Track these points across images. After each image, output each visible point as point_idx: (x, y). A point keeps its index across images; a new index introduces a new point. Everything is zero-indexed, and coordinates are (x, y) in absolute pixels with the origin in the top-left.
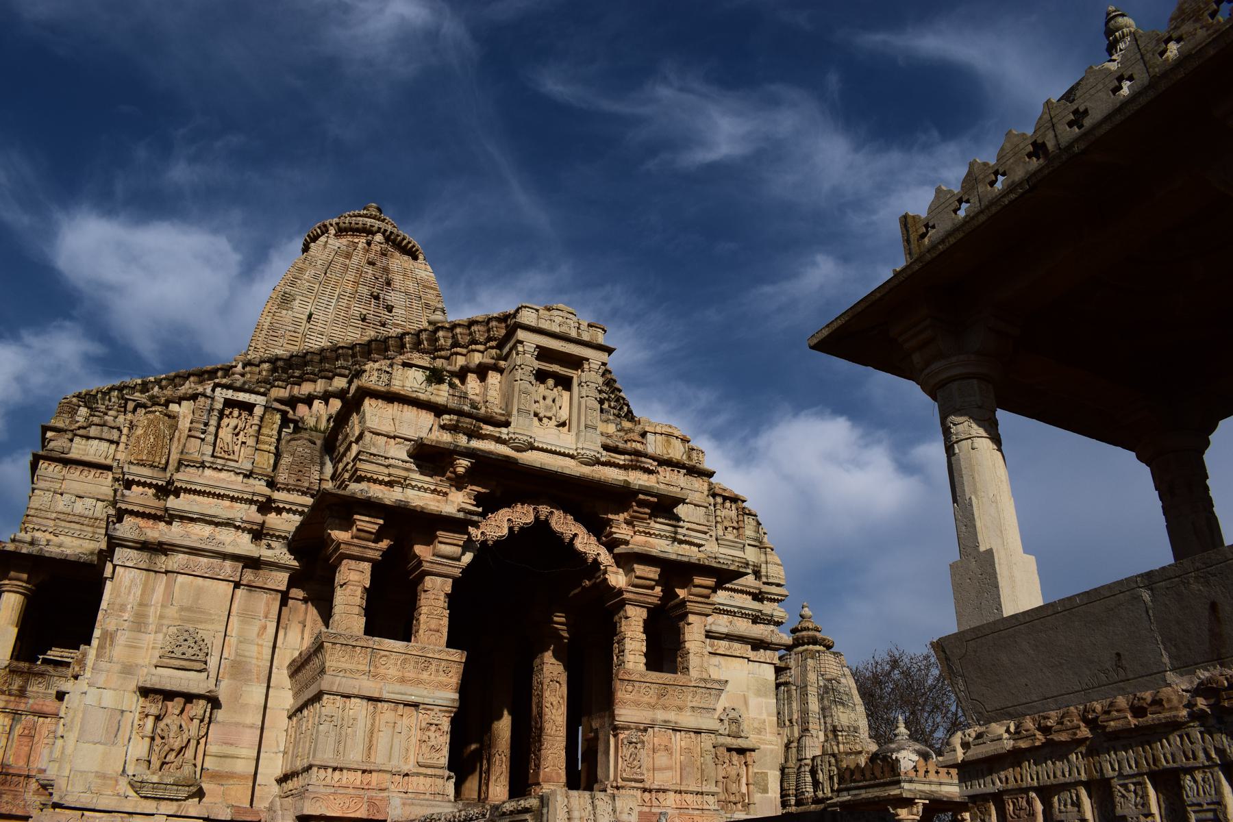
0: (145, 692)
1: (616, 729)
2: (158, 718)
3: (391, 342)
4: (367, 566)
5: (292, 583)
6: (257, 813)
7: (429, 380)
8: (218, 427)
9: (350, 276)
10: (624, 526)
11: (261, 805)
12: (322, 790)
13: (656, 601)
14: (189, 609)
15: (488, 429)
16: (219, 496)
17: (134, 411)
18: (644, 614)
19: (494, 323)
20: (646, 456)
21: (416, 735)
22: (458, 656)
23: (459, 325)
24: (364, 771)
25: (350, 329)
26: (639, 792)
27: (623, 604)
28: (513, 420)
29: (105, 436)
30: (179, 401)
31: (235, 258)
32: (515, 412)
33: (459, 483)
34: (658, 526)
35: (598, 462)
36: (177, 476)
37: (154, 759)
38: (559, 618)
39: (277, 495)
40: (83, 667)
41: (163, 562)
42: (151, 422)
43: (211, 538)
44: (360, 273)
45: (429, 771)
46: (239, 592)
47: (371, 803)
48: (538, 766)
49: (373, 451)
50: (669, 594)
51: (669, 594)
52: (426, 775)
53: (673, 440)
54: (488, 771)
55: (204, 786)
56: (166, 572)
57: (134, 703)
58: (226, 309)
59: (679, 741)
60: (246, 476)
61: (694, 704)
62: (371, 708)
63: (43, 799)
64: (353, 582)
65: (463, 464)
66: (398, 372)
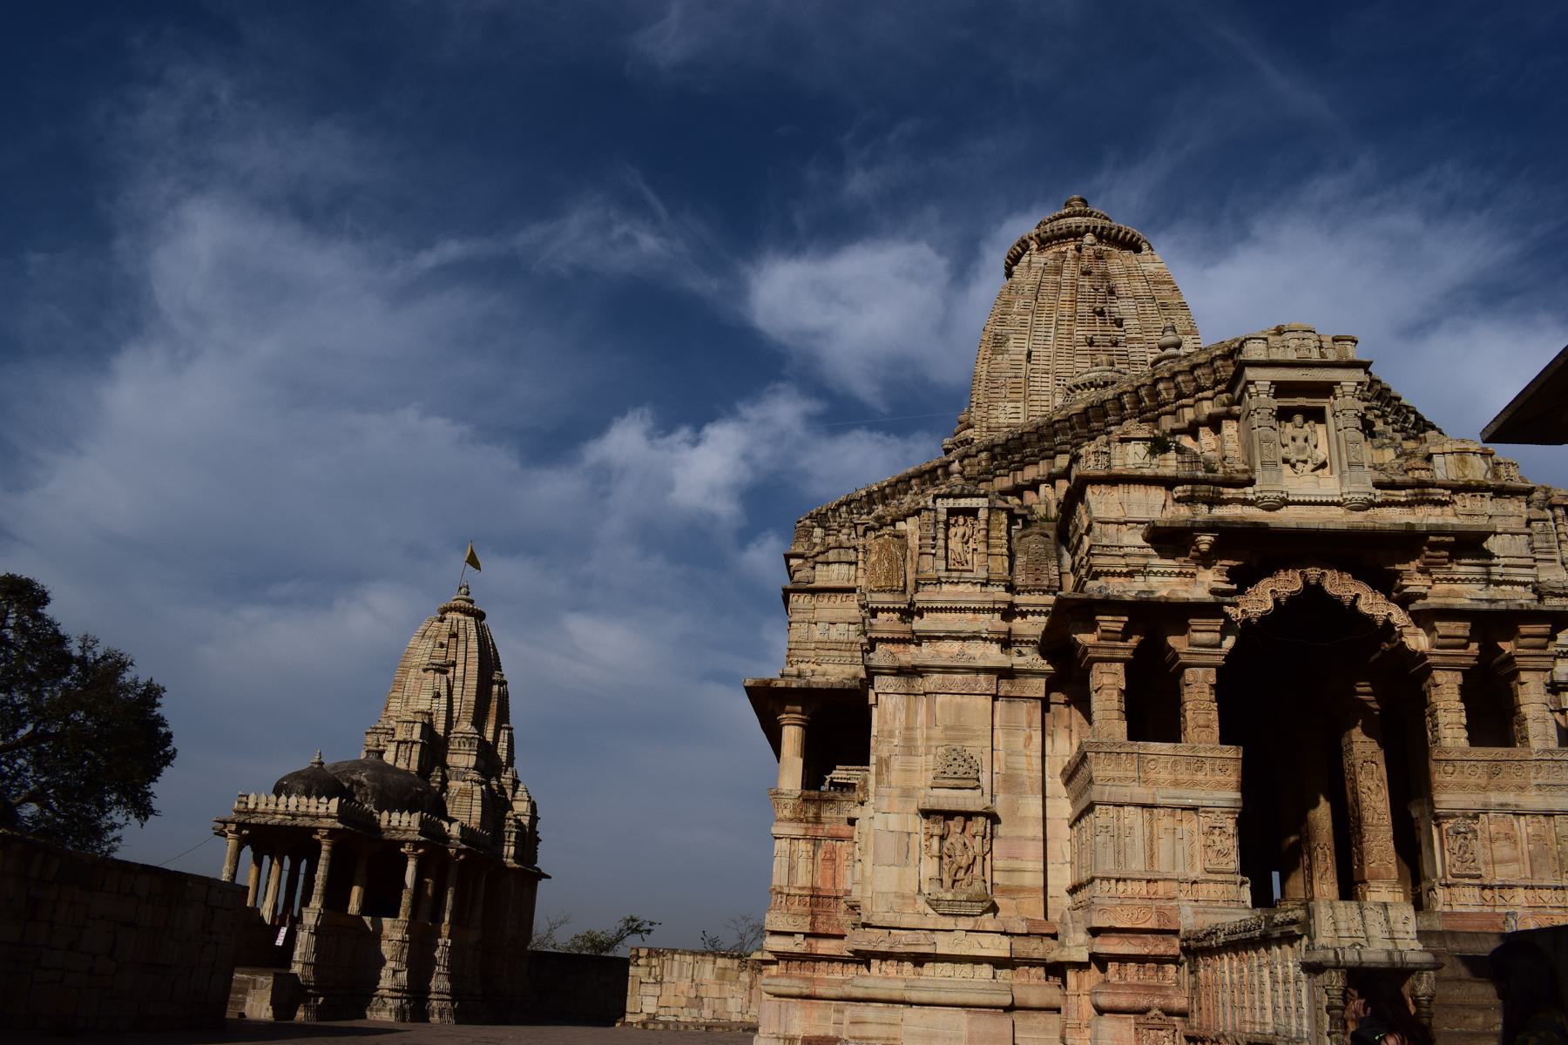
0: (926, 814)
1: (1438, 819)
2: (942, 838)
3: (1109, 406)
4: (1119, 667)
5: (1050, 688)
6: (1053, 925)
7: (1152, 452)
8: (947, 538)
9: (1065, 295)
10: (1419, 576)
11: (1054, 917)
12: (1108, 901)
13: (1471, 661)
14: (952, 728)
15: (1230, 492)
16: (961, 610)
17: (864, 535)
18: (1458, 678)
19: (1218, 363)
20: (1434, 485)
21: (1200, 841)
22: (1233, 752)
23: (1180, 372)
24: (1149, 881)
25: (1077, 359)
26: (1477, 890)
27: (1428, 670)
28: (1258, 476)
29: (843, 558)
30: (904, 518)
31: (941, 264)
32: (1258, 466)
33: (1206, 561)
34: (1462, 569)
35: (1372, 504)
36: (917, 597)
37: (945, 877)
38: (1363, 688)
39: (1018, 599)
40: (866, 793)
41: (921, 684)
42: (882, 546)
43: (961, 654)
44: (1075, 287)
45: (1219, 877)
46: (998, 704)
47: (1161, 913)
48: (1361, 861)
49: (1105, 542)
50: (1490, 650)
51: (1490, 650)
52: (1216, 882)
53: (1470, 458)
54: (1310, 868)
55: (997, 901)
56: (925, 694)
57: (918, 825)
58: (944, 327)
59: (1524, 827)
60: (983, 585)
61: (1540, 781)
62: (1147, 815)
63: (854, 918)
64: (1108, 682)
65: (1205, 542)
66: (1117, 450)
